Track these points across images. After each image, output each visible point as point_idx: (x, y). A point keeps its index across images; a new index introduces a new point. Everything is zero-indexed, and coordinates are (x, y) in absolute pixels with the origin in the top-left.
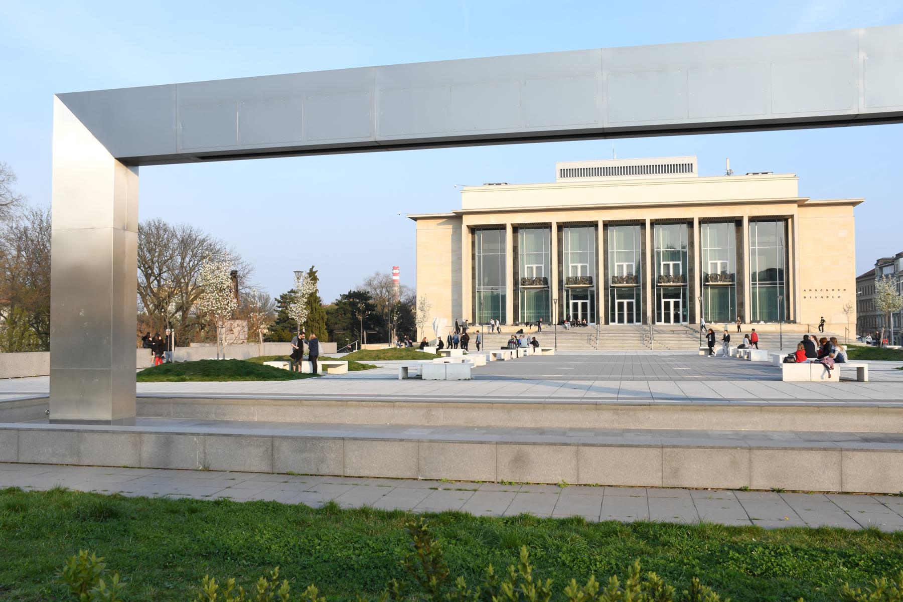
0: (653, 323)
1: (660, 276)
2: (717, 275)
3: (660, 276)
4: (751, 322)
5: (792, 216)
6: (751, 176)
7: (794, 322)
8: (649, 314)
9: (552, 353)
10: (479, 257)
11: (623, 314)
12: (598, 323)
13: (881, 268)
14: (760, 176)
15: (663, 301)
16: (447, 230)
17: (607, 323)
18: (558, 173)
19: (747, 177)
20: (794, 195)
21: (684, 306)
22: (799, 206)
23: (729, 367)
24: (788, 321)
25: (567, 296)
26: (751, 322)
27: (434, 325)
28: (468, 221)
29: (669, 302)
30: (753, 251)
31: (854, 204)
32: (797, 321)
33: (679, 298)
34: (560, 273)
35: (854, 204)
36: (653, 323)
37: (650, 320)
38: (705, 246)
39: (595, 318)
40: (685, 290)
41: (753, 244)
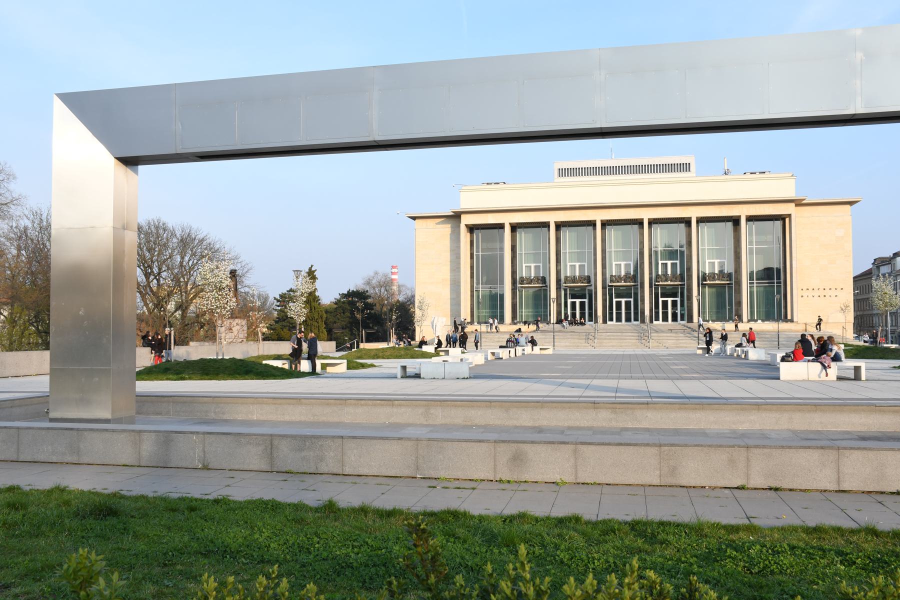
0: (651, 322)
1: (657, 275)
2: (714, 274)
3: (657, 275)
4: (749, 321)
5: (789, 216)
6: (748, 176)
7: (792, 321)
8: (647, 313)
9: (550, 351)
10: (478, 256)
11: (621, 313)
12: (596, 322)
13: (878, 267)
14: (758, 175)
15: (661, 300)
16: (446, 229)
17: (605, 322)
18: (556, 173)
19: (745, 176)
20: (791, 194)
21: (682, 305)
22: (796, 205)
23: (727, 366)
24: (786, 320)
25: (566, 295)
26: (749, 321)
27: (432, 324)
28: (467, 220)
29: (667, 301)
30: (751, 251)
31: (851, 203)
32: (795, 320)
33: (676, 297)
34: (558, 273)
35: (851, 203)
36: (651, 322)
38: (703, 245)
39: (593, 317)
40: (682, 289)
41: (751, 243)
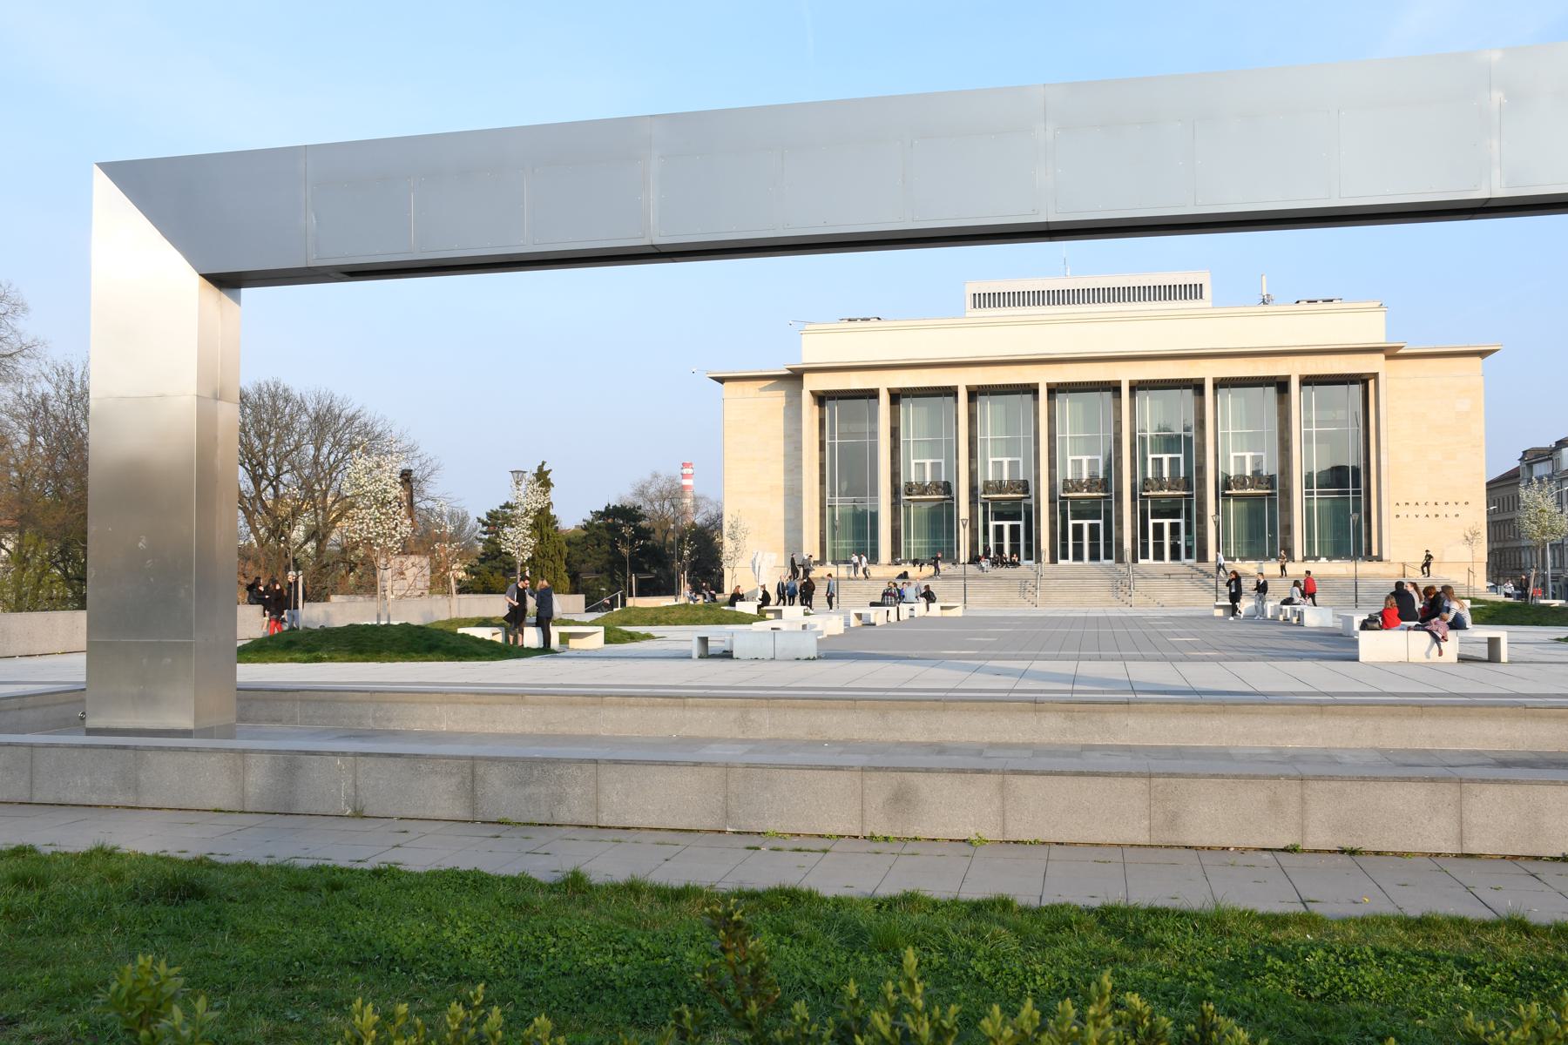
0: (1135, 560)
1: (1145, 480)
2: (1244, 477)
3: (1145, 480)
4: (1304, 559)
5: (1375, 376)
6: (1304, 306)
7: (1379, 559)
8: (1127, 544)
9: (958, 612)
10: (832, 446)
11: (1081, 546)
12: (1039, 560)
13: (1530, 466)
14: (1320, 306)
15: (1151, 522)
16: (777, 399)
17: (1053, 560)
18: (969, 300)
19: (1297, 307)
20: (1378, 338)
21: (1188, 531)
22: (1388, 358)
24: (1369, 557)
25: (985, 514)
26: (1304, 559)
27: (753, 563)
28: (813, 383)
29: (1162, 525)
30: (1308, 436)
31: (1482, 354)
32: (1385, 557)
33: (1178, 517)
34: (973, 475)
35: (1482, 354)
36: (1135, 560)
37: (1128, 556)
38: (1225, 426)
39: (1032, 552)
40: (1189, 503)
41: (1308, 423)
